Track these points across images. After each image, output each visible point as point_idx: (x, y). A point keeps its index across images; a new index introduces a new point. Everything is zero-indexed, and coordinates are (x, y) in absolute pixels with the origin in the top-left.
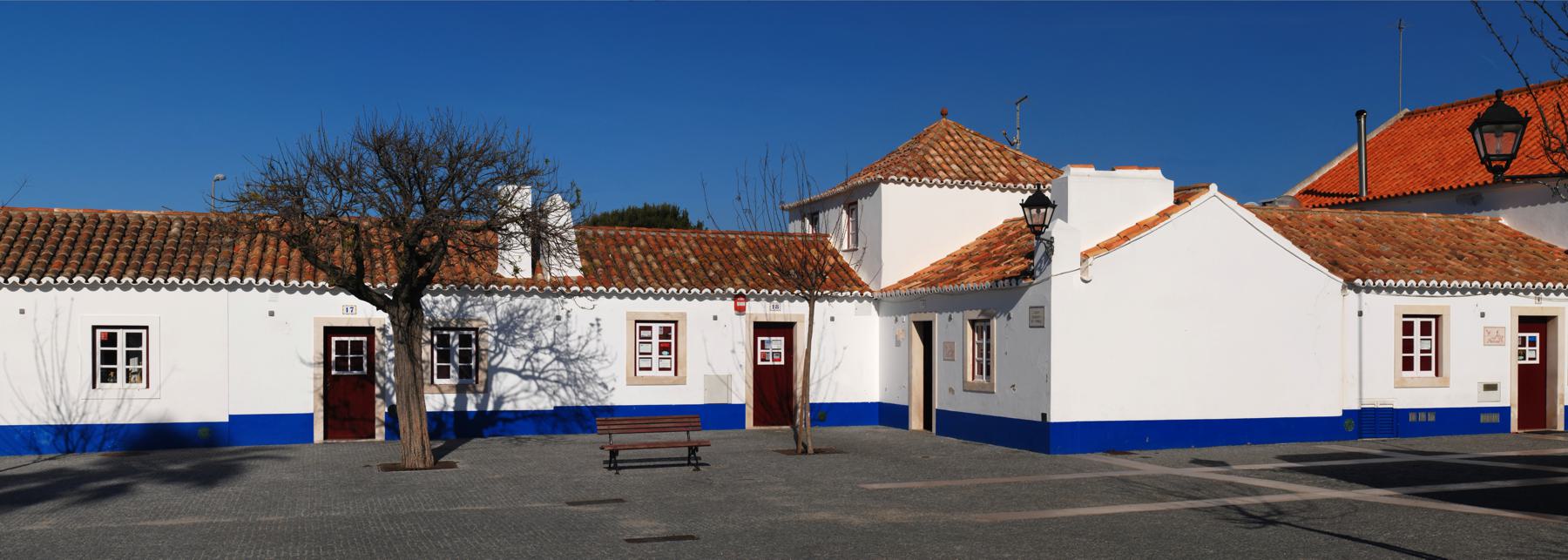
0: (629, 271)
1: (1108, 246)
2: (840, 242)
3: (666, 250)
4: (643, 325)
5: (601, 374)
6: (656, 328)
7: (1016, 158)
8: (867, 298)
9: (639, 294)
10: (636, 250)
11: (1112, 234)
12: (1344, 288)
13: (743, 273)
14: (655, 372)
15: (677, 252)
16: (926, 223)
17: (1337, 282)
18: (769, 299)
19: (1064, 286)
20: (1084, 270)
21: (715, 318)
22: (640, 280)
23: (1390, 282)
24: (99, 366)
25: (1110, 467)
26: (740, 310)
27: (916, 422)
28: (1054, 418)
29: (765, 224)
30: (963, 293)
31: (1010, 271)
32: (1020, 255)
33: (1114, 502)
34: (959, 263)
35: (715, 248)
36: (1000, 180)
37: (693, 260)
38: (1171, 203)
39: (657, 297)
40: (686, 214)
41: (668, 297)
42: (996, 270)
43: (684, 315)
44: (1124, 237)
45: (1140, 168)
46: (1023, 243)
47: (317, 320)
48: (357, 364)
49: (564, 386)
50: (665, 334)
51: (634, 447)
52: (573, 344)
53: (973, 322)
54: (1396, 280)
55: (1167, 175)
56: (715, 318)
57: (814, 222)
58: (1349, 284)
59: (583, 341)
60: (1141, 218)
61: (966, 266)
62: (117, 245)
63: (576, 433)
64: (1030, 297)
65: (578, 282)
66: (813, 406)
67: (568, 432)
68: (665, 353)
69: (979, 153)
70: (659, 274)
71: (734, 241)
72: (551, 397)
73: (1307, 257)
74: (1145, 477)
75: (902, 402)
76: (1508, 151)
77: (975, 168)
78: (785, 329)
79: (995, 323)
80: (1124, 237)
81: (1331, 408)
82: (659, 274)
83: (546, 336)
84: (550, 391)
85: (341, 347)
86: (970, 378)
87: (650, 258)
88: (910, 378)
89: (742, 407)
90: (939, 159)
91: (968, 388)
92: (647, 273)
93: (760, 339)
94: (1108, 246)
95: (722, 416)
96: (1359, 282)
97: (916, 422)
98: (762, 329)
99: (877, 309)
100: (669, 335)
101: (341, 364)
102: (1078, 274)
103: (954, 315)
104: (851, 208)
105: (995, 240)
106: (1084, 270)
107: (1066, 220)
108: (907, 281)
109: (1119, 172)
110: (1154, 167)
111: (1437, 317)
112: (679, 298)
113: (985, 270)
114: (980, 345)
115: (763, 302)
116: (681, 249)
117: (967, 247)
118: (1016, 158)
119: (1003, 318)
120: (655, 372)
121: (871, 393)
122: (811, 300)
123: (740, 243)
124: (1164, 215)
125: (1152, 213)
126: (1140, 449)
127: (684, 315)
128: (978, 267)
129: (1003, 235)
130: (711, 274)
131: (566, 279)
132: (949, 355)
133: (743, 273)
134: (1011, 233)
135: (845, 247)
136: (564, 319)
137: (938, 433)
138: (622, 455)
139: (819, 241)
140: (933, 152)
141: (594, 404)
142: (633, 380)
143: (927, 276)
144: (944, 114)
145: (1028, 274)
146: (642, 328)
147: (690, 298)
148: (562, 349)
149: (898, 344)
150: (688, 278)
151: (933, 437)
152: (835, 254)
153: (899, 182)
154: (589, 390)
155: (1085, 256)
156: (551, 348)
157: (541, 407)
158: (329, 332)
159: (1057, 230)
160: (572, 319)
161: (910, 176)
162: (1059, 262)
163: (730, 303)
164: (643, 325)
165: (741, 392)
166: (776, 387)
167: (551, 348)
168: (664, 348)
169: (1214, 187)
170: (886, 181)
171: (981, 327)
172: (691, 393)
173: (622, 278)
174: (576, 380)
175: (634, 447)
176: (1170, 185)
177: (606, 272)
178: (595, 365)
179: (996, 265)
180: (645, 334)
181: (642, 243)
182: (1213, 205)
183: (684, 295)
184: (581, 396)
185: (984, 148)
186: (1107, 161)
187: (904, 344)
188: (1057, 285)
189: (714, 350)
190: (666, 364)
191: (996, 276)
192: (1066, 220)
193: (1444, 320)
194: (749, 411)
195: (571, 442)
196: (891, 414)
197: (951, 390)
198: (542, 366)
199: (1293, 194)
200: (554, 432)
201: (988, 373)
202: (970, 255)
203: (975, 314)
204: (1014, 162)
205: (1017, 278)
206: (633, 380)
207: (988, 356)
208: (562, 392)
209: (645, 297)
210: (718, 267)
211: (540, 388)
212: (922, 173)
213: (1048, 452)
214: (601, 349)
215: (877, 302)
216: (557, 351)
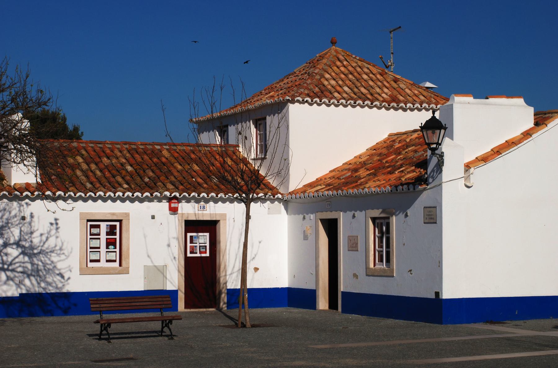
0: (78, 177)
1: (485, 159)
2: (249, 150)
3: (105, 159)
4: (93, 224)
5: (59, 266)
7: (396, 81)
8: (279, 200)
9: (90, 197)
10: (80, 160)
11: (487, 149)
13: (173, 178)
15: (114, 161)
16: (326, 137)
18: (198, 201)
20: (467, 178)
21: (153, 217)
22: (89, 185)
25: (494, 332)
26: (174, 211)
27: (323, 303)
28: (446, 295)
29: (182, 134)
30: (361, 196)
31: (404, 177)
32: (411, 164)
33: (506, 352)
34: (356, 170)
35: (146, 157)
37: (129, 168)
38: (532, 125)
39: (105, 200)
40: (64, 119)
41: (114, 200)
42: (393, 177)
43: (127, 215)
44: (497, 152)
45: (508, 97)
46: (411, 155)
49: (29, 276)
50: (111, 231)
51: (123, 321)
52: (36, 241)
53: (374, 220)
56: (153, 217)
57: (223, 133)
59: (44, 238)
61: (362, 173)
63: (38, 316)
64: (425, 198)
65: (39, 187)
66: (228, 290)
67: (32, 315)
68: (111, 247)
69: (365, 77)
70: (103, 180)
72: (18, 286)
74: (522, 337)
75: (309, 285)
77: (363, 90)
78: (210, 227)
79: (394, 219)
80: (497, 152)
82: (103, 180)
83: (15, 233)
84: (17, 280)
86: (372, 265)
87: (93, 166)
88: (317, 266)
89: (175, 292)
90: (333, 82)
91: (370, 273)
92: (93, 179)
93: (189, 235)
94: (485, 159)
95: (159, 299)
97: (323, 303)
98: (192, 226)
99: (286, 209)
100: (115, 232)
103: (357, 214)
104: (260, 123)
105: (384, 151)
106: (467, 178)
107: (452, 138)
109: (491, 100)
110: (519, 96)
111: (120, 221)
112: (123, 200)
115: (193, 204)
117: (360, 156)
118: (396, 81)
119: (402, 216)
120: (103, 264)
122: (248, 203)
123: (165, 153)
124: (527, 134)
126: (511, 319)
127: (127, 215)
129: (394, 145)
130: (147, 180)
131: (28, 185)
132: (353, 246)
133: (173, 178)
134: (397, 145)
135: (253, 156)
136: (28, 219)
137: (344, 311)
138: (114, 328)
139: (228, 151)
140: (327, 76)
141: (53, 291)
142: (84, 271)
144: (333, 43)
145: (422, 180)
146: (92, 226)
147: (132, 200)
148: (27, 245)
149: (306, 238)
150: (128, 184)
151: (339, 315)
152: (245, 161)
153: (303, 102)
154: (49, 279)
155: (468, 167)
156: (18, 244)
157: (9, 294)
158: (436, 223)
159: (447, 147)
160: (35, 219)
162: (447, 173)
163: (165, 205)
164: (93, 224)
165: (174, 280)
166: (201, 272)
167: (18, 244)
168: (110, 243)
170: (293, 102)
171: (383, 226)
172: (133, 282)
173: (74, 185)
174: (38, 271)
175: (123, 321)
177: (58, 181)
178: (54, 258)
179: (391, 173)
180: (95, 231)
181: (84, 152)
183: (128, 198)
184: (43, 285)
185: (369, 72)
186: (482, 92)
187: (312, 238)
188: (446, 188)
189: (152, 243)
190: (112, 256)
191: (393, 181)
192: (452, 138)
193: (124, 223)
194: (181, 296)
195: (42, 323)
196: (299, 297)
197: (355, 276)
198: (10, 259)
200: (20, 316)
201: (388, 260)
203: (376, 213)
204: (395, 85)
205: (414, 184)
206: (84, 271)
207: (388, 246)
208: (27, 282)
209: (95, 200)
210: (151, 174)
211: (9, 278)
212: (320, 94)
213: (441, 323)
214: (59, 244)
215: (286, 203)
216: (23, 247)
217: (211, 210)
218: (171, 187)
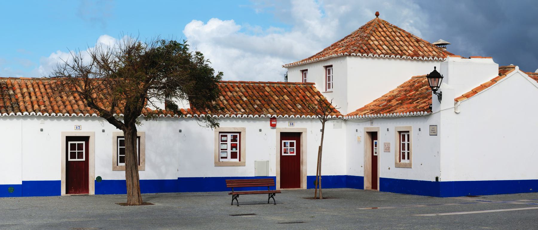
1: (467, 96)
2: (320, 87)
3: (229, 94)
6: (229, 136)
11: (469, 90)
13: (273, 106)
14: (229, 160)
15: (235, 94)
19: (444, 113)
24: (119, 155)
26: (273, 126)
27: (367, 184)
28: (442, 179)
34: (390, 101)
36: (409, 55)
37: (245, 99)
38: (497, 75)
44: (475, 92)
47: (62, 133)
48: (80, 155)
50: (234, 139)
55: (495, 61)
60: (483, 83)
61: (394, 102)
69: (397, 39)
71: (264, 87)
77: (396, 47)
78: (297, 136)
80: (475, 92)
82: (228, 106)
85: (80, 147)
90: (376, 43)
93: (283, 141)
94: (467, 96)
97: (367, 184)
98: (284, 136)
101: (73, 156)
102: (453, 110)
105: (408, 88)
106: (455, 108)
108: (361, 110)
116: (237, 92)
117: (393, 91)
121: (343, 170)
124: (494, 81)
125: (488, 80)
127: (244, 129)
128: (401, 104)
130: (256, 106)
134: (416, 84)
137: (381, 190)
139: (309, 87)
140: (372, 38)
143: (372, 107)
146: (222, 136)
152: (318, 94)
155: (456, 100)
158: (68, 139)
161: (362, 53)
165: (274, 170)
166: (291, 166)
168: (233, 146)
172: (248, 170)
176: (497, 66)
179: (411, 103)
180: (224, 138)
182: (517, 77)
194: (278, 179)
196: (353, 182)
204: (417, 44)
206: (218, 164)
210: (258, 102)
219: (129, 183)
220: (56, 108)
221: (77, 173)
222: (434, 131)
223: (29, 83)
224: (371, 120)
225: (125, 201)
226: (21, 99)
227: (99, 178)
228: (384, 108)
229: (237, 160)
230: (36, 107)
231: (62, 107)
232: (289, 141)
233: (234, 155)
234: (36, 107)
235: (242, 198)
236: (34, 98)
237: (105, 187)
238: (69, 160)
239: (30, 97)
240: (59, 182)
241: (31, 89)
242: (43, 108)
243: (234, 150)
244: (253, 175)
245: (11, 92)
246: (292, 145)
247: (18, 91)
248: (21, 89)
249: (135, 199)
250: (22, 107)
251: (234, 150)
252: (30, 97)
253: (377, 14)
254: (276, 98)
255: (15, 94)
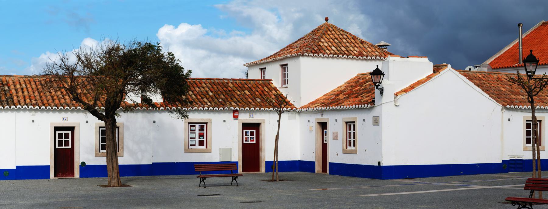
1: (406, 91)
2: (276, 83)
3: (197, 89)
12: (502, 109)
13: (235, 100)
14: (197, 147)
15: (202, 89)
17: (499, 107)
19: (386, 106)
23: (521, 106)
24: (101, 143)
26: (236, 117)
27: (318, 168)
36: (355, 55)
37: (211, 94)
44: (412, 87)
48: (67, 144)
50: (202, 129)
54: (523, 106)
55: (430, 60)
58: (505, 106)
60: (419, 79)
61: (341, 96)
62: (46, 97)
69: (344, 41)
71: (227, 83)
73: (488, 96)
76: (533, 71)
78: (256, 126)
80: (412, 87)
81: (497, 160)
85: (67, 136)
89: (237, 162)
90: (326, 44)
93: (244, 131)
94: (406, 91)
96: (508, 106)
97: (318, 168)
98: (245, 126)
101: (60, 144)
105: (354, 84)
108: (313, 103)
113: (351, 100)
114: (350, 133)
116: (204, 88)
124: (429, 77)
125: (424, 77)
127: (210, 120)
128: (348, 98)
130: (220, 100)
133: (235, 100)
134: (361, 81)
139: (267, 83)
140: (323, 40)
143: (322, 101)
146: (191, 126)
152: (275, 89)
155: (396, 95)
158: (56, 129)
165: (236, 156)
166: (251, 152)
168: (201, 135)
169: (449, 66)
172: (214, 156)
176: (431, 65)
179: (356, 97)
180: (192, 128)
182: (449, 74)
193: (543, 123)
194: (240, 164)
196: (305, 166)
199: (488, 63)
202: (342, 92)
204: (361, 46)
206: (187, 151)
210: (223, 97)
217: (256, 118)
218: (234, 104)
219: (109, 167)
220: (45, 102)
221: (64, 158)
222: (376, 122)
223: (21, 80)
224: (322, 112)
225: (106, 183)
226: (14, 94)
227: (83, 163)
228: (333, 101)
229: (204, 147)
230: (28, 101)
231: (50, 101)
232: (250, 131)
233: (201, 143)
234: (28, 101)
235: (208, 181)
236: (26, 93)
237: (88, 171)
238: (57, 147)
239: (23, 92)
240: (48, 167)
241: (24, 85)
242: (34, 102)
243: (202, 139)
244: (218, 160)
245: (6, 88)
246: (252, 134)
247: (12, 87)
248: (15, 86)
249: (115, 181)
250: (16, 101)
251: (202, 139)
252: (23, 92)
253: (327, 19)
254: (239, 93)
255: (10, 90)
